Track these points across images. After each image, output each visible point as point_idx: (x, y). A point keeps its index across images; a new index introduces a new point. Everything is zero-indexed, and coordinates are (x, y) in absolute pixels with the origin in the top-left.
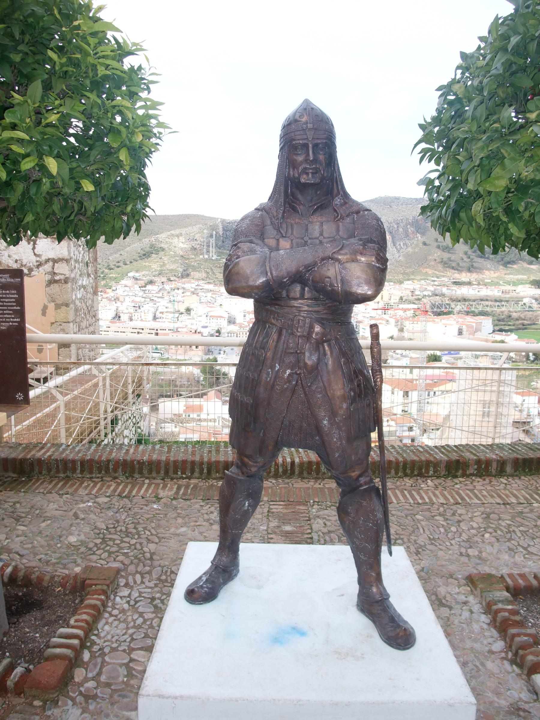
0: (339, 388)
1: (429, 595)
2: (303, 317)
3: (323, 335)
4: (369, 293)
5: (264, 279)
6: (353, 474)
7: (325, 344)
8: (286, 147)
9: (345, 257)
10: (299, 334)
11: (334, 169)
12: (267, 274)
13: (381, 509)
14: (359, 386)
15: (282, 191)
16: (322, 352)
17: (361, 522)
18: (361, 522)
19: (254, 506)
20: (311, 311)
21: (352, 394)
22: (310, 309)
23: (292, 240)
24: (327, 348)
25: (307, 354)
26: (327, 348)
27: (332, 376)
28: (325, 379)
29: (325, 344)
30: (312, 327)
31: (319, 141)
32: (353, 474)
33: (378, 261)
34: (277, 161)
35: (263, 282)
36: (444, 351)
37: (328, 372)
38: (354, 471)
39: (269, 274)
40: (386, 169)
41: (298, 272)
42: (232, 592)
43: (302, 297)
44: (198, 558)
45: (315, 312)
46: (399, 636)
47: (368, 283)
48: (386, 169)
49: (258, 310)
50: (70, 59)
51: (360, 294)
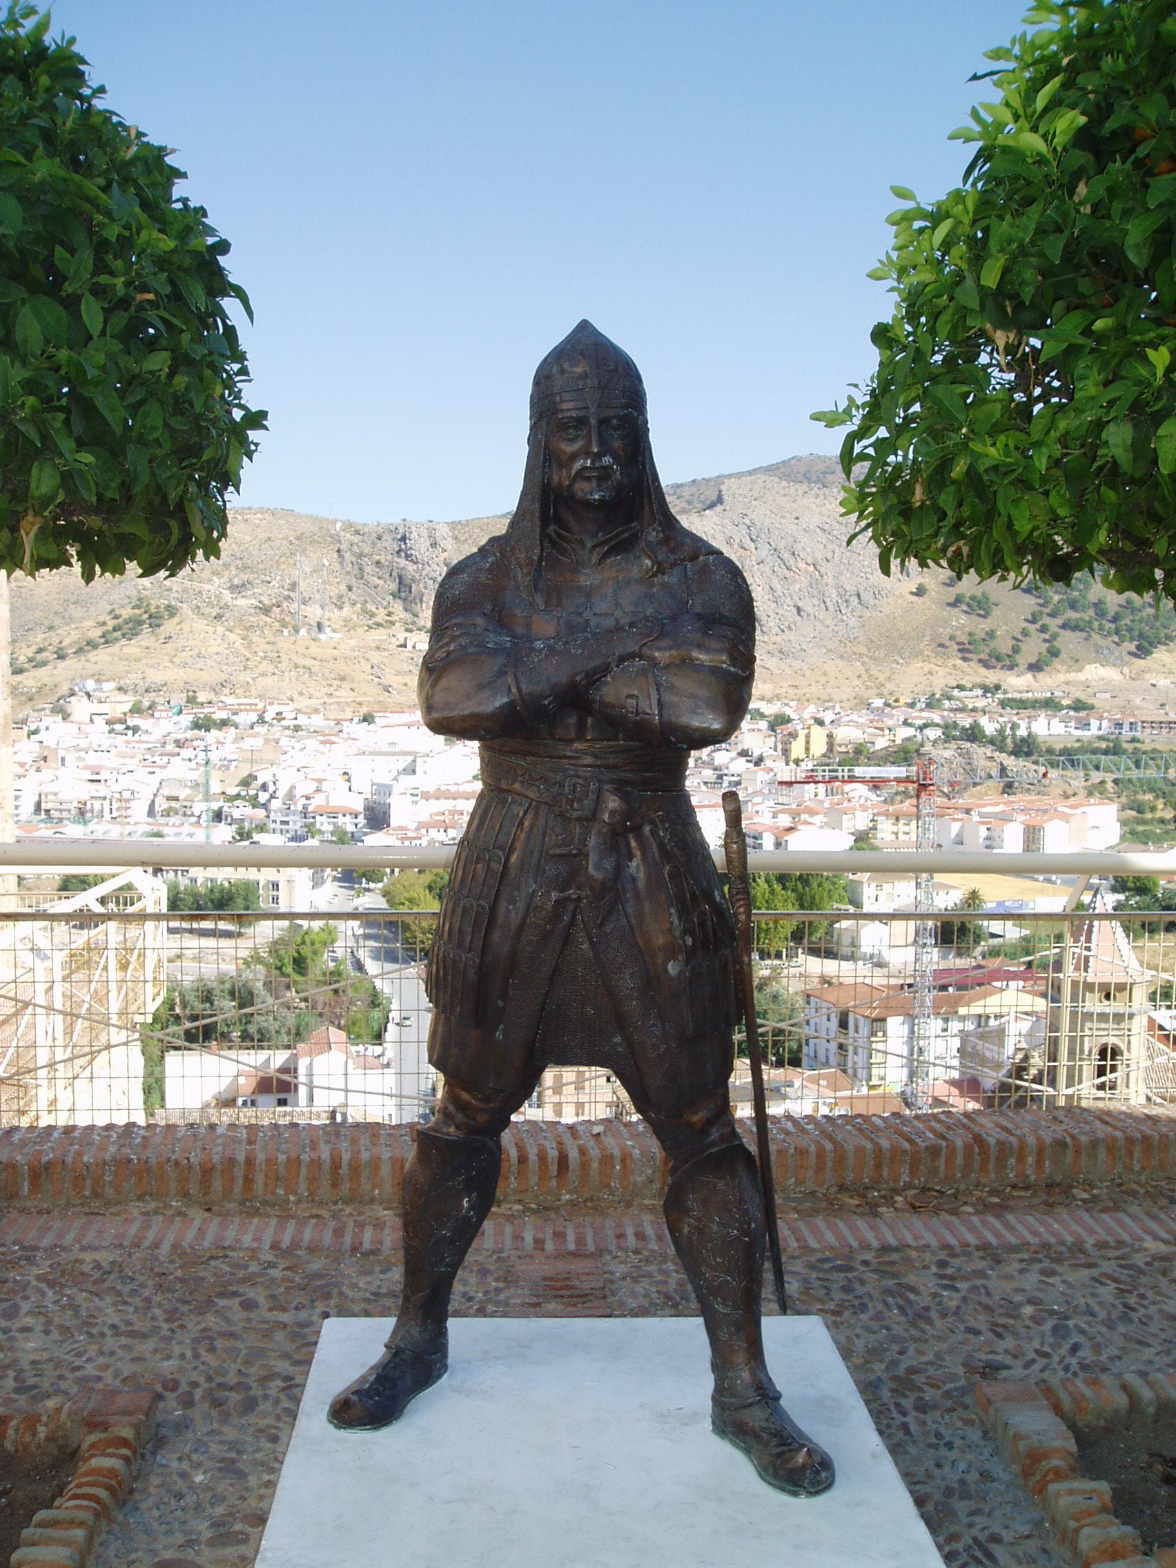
0: (662, 926)
1: (941, 1539)
2: (584, 778)
3: (628, 814)
4: (716, 726)
5: (505, 700)
6: (695, 1119)
7: (630, 836)
8: (544, 423)
9: (667, 654)
10: (575, 814)
11: (644, 467)
12: (510, 690)
13: (757, 1200)
14: (702, 924)
15: (537, 514)
16: (624, 852)
17: (715, 1228)
18: (715, 1228)
19: (483, 1208)
20: (598, 766)
21: (689, 941)
22: (599, 762)
23: (558, 618)
24: (633, 844)
25: (593, 858)
26: (633, 844)
27: (646, 904)
28: (630, 910)
29: (630, 836)
30: (598, 800)
31: (611, 413)
32: (695, 1119)
33: (733, 660)
34: (525, 449)
35: (502, 707)
36: (959, 828)
37: (637, 894)
38: (697, 1113)
39: (514, 690)
40: (757, 426)
41: (573, 685)
42: (432, 1414)
43: (580, 737)
44: (351, 1346)
45: (608, 767)
46: (795, 1466)
47: (712, 707)
48: (757, 426)
49: (492, 770)
50: (863, 1196)
51: (698, 729)
